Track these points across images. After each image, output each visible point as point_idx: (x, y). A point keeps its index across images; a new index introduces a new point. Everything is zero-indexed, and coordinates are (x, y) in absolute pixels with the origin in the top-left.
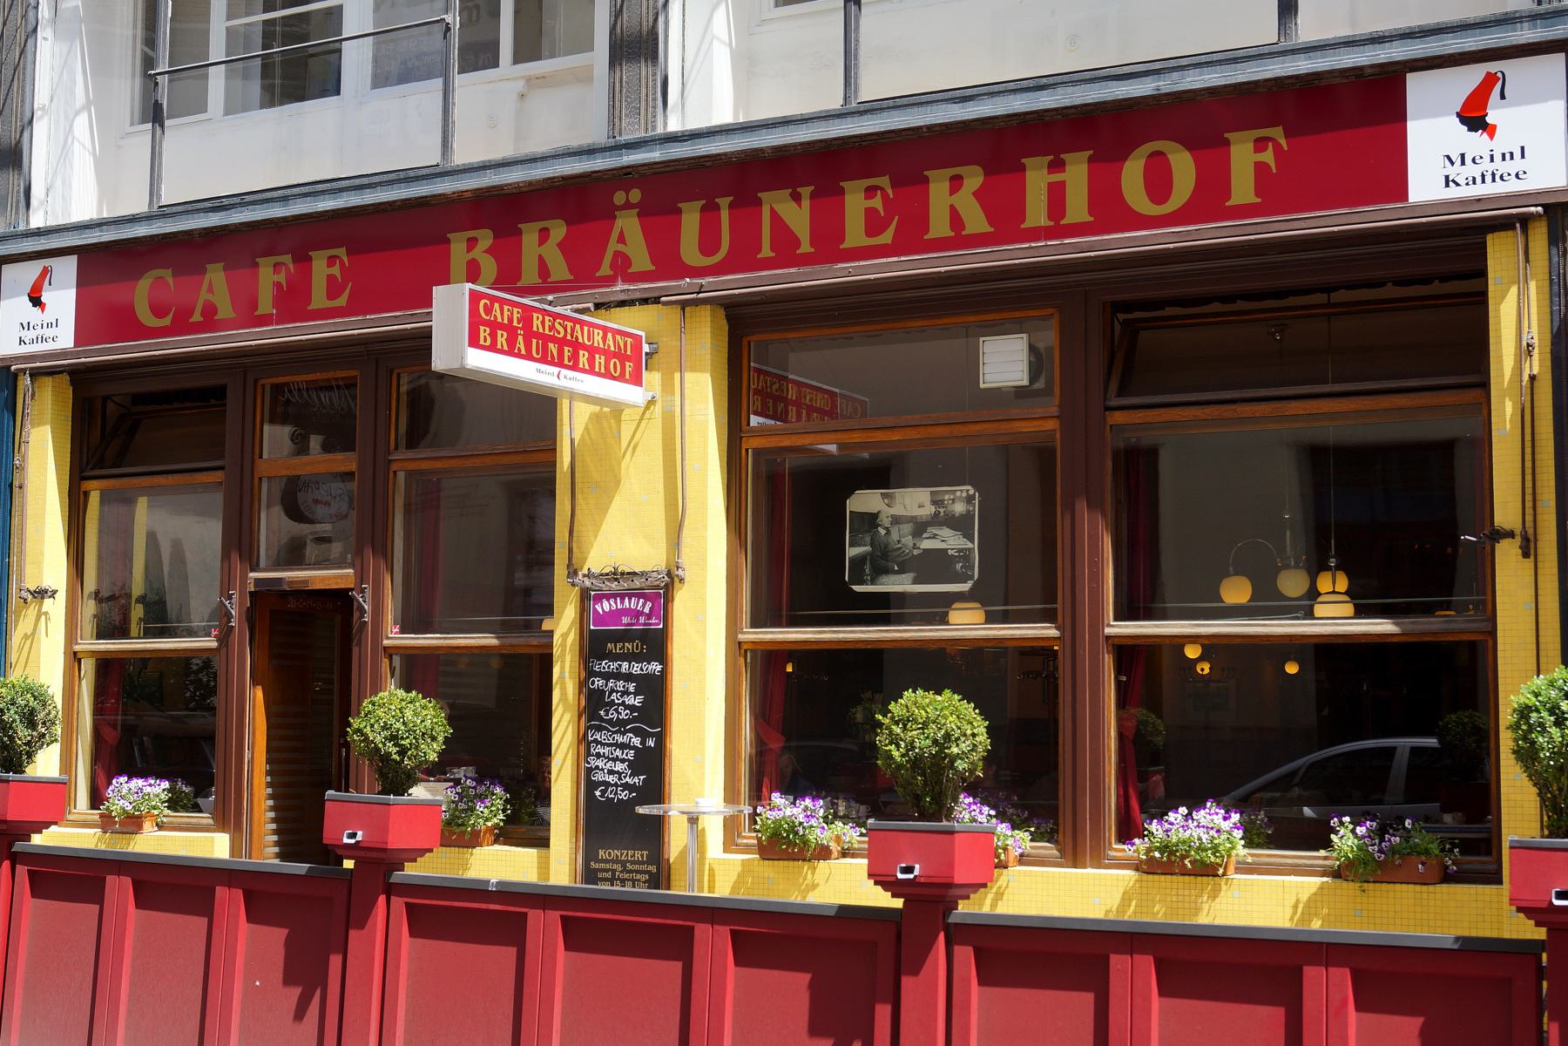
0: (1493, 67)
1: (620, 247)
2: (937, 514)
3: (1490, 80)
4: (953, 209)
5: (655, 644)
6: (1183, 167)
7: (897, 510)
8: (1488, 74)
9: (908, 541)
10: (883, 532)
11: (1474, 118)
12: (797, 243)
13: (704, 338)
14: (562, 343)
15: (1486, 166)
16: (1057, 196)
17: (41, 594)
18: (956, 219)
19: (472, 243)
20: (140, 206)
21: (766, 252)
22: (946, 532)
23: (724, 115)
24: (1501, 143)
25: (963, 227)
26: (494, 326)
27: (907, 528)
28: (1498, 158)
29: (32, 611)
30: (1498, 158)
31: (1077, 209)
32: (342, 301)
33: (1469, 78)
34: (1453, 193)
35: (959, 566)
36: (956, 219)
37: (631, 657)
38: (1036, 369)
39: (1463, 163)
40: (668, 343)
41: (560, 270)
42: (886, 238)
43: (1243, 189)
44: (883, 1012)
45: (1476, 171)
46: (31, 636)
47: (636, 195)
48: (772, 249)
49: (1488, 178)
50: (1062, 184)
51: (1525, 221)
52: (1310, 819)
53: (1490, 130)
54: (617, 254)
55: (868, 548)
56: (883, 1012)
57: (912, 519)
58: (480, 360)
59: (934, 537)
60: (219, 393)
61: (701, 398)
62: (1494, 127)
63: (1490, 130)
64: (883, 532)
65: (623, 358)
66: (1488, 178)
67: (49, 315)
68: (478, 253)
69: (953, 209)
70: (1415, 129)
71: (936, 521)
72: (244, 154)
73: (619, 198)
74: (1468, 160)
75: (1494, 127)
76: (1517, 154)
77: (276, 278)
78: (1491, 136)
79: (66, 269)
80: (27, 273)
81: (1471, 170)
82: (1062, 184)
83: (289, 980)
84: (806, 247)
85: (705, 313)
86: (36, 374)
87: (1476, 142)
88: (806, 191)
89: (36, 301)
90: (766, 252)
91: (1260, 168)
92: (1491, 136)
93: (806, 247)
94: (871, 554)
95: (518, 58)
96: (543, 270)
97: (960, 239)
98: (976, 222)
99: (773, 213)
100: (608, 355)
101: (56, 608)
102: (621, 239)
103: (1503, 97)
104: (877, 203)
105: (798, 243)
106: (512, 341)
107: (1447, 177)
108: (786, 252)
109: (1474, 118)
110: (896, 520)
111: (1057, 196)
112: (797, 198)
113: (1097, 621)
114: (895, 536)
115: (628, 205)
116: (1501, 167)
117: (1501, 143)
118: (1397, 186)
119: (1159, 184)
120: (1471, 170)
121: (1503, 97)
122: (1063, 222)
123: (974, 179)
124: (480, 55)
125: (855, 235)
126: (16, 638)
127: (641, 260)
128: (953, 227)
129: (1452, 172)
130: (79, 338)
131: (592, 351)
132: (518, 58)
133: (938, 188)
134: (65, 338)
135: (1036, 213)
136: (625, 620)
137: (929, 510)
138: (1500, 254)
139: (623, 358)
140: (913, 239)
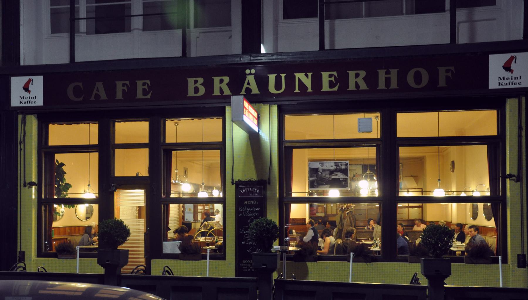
1: (97, 92)
2: (337, 169)
4: (220, 88)
7: (325, 167)
8: (512, 56)
9: (328, 176)
10: (320, 173)
15: (510, 80)
16: (388, 81)
18: (221, 91)
19: (196, 82)
21: (297, 90)
22: (339, 174)
24: (515, 75)
25: (223, 93)
27: (327, 172)
28: (513, 78)
30: (513, 78)
32: (149, 96)
34: (501, 87)
35: (343, 183)
36: (221, 91)
39: (504, 79)
42: (336, 89)
45: (507, 82)
48: (95, 98)
49: (511, 84)
50: (390, 78)
52: (295, 251)
53: (512, 71)
54: (96, 94)
55: (316, 178)
57: (329, 170)
59: (336, 175)
62: (513, 70)
63: (512, 71)
64: (320, 173)
66: (511, 84)
67: (32, 94)
68: (198, 85)
69: (220, 88)
71: (336, 170)
73: (248, 71)
74: (505, 78)
75: (513, 70)
76: (519, 78)
77: (123, 88)
78: (512, 73)
81: (25, 100)
82: (390, 78)
84: (310, 90)
88: (310, 74)
90: (297, 90)
92: (512, 73)
93: (310, 90)
94: (317, 180)
102: (98, 90)
103: (515, 62)
105: (307, 89)
107: (499, 83)
110: (324, 170)
112: (307, 76)
114: (324, 175)
115: (250, 74)
116: (515, 81)
117: (515, 75)
120: (25, 100)
121: (515, 62)
122: (390, 88)
128: (356, 88)
129: (21, 100)
136: (250, 195)
137: (334, 167)
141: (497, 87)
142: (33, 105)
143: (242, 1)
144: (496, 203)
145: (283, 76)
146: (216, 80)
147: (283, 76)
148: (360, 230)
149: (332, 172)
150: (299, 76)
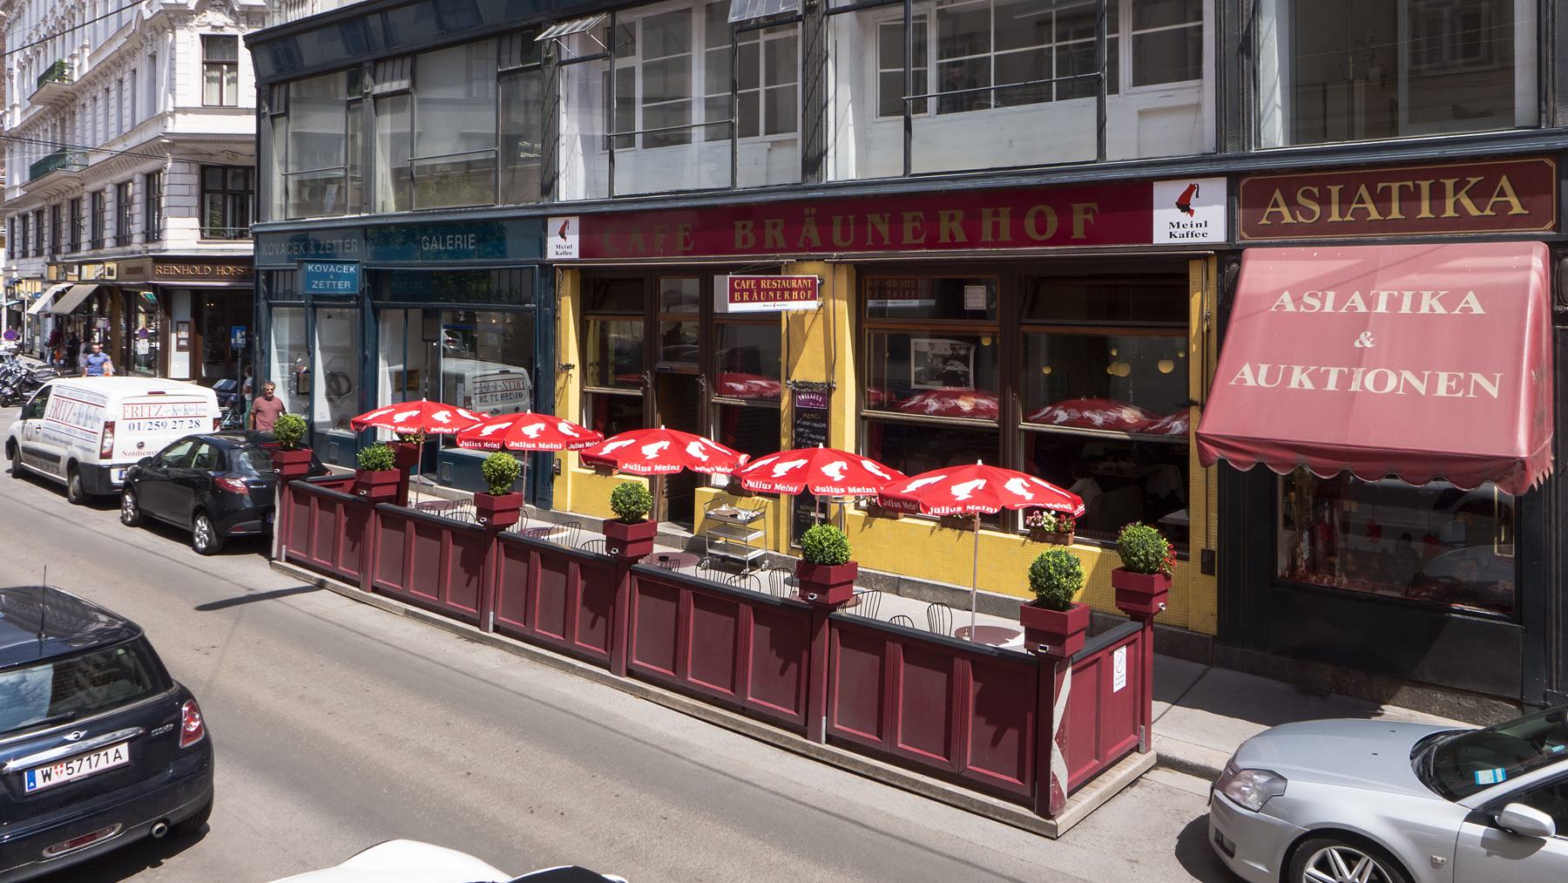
0: (1193, 182)
3: (1192, 188)
5: (824, 416)
6: (1053, 223)
11: (1184, 205)
12: (882, 239)
13: (843, 282)
14: (775, 290)
15: (1189, 229)
16: (996, 226)
17: (569, 367)
20: (604, 195)
21: (870, 242)
22: (957, 363)
23: (852, 175)
26: (742, 291)
29: (563, 376)
31: (1005, 235)
33: (1183, 186)
37: (813, 420)
38: (989, 301)
40: (828, 278)
41: (782, 243)
43: (1078, 232)
44: (805, 654)
45: (1184, 231)
46: (564, 387)
47: (813, 211)
51: (1206, 258)
53: (1191, 212)
56: (805, 654)
58: (734, 308)
60: (642, 280)
61: (842, 310)
63: (1191, 212)
65: (806, 289)
67: (568, 242)
70: (1157, 214)
72: (646, 174)
73: (807, 211)
79: (574, 223)
80: (559, 222)
81: (1182, 231)
83: (886, 111)
84: (887, 242)
85: (844, 267)
86: (562, 268)
87: (1184, 218)
88: (887, 216)
89: (563, 236)
90: (870, 242)
91: (1086, 222)
93: (887, 242)
95: (767, 133)
96: (775, 242)
97: (953, 244)
98: (961, 237)
99: (874, 229)
100: (799, 290)
101: (575, 373)
104: (918, 224)
106: (751, 296)
108: (878, 244)
109: (1184, 205)
110: (935, 356)
111: (996, 226)
113: (1015, 423)
118: (1148, 236)
119: (1041, 229)
120: (1182, 231)
123: (959, 214)
124: (750, 130)
125: (908, 238)
126: (559, 384)
127: (816, 242)
129: (1173, 230)
130: (582, 254)
131: (791, 290)
132: (767, 133)
133: (944, 215)
134: (575, 255)
135: (987, 235)
137: (950, 352)
138: (1195, 273)
139: (806, 289)
140: (932, 243)
141: (1166, 240)
142: (1201, 240)
143: (1134, 5)
144: (503, 311)
145: (851, 218)
146: (944, 215)
147: (851, 218)
148: (31, 220)
149: (946, 360)
150: (873, 218)
